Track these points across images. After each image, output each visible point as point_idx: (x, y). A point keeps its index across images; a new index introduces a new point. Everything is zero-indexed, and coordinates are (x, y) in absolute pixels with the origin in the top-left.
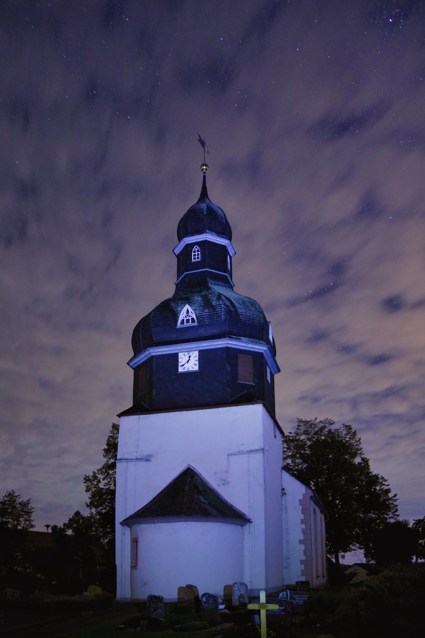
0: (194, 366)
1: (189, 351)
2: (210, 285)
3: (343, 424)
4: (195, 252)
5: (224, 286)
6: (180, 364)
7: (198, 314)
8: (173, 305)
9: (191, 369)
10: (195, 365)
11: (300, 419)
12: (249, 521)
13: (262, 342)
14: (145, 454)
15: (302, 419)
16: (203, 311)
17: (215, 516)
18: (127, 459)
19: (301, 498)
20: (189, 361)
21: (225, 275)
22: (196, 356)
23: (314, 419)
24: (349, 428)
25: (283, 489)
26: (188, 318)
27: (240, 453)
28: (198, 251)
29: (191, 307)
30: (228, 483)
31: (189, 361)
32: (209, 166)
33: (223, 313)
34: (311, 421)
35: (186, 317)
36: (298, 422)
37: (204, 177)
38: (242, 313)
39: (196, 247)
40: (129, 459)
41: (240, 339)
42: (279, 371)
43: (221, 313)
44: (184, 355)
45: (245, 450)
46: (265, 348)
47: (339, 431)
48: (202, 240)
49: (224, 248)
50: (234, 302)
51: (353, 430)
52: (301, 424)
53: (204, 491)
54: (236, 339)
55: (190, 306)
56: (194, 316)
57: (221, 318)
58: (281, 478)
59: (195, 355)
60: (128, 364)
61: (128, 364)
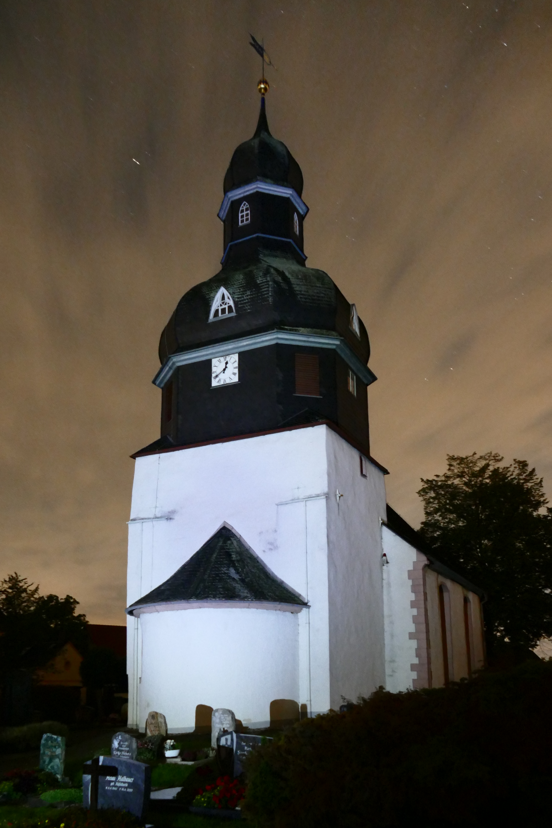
0: (232, 376)
1: (226, 354)
2: (261, 256)
3: (515, 460)
4: (242, 211)
5: (285, 257)
6: (214, 375)
7: (236, 299)
8: (205, 290)
9: (228, 381)
10: (234, 374)
11: (451, 455)
12: (305, 605)
13: (334, 333)
14: (167, 509)
15: (454, 456)
16: (244, 294)
17: (243, 599)
18: (143, 519)
19: (411, 568)
20: (225, 371)
21: (264, 234)
22: (235, 361)
23: (471, 454)
24: (523, 465)
25: (385, 555)
26: (223, 306)
27: (295, 500)
28: (247, 210)
29: (228, 291)
30: (276, 548)
31: (225, 371)
32: (268, 81)
33: (270, 294)
34: (467, 458)
35: (221, 305)
36: (448, 459)
37: (263, 100)
38: (301, 291)
39: (245, 204)
40: (145, 519)
41: (296, 330)
42: (374, 379)
43: (268, 294)
44: (220, 361)
45: (302, 497)
46: (338, 342)
47: (509, 469)
48: (252, 192)
49: (287, 200)
50: (289, 276)
51: (529, 469)
52: (455, 463)
53: (238, 561)
54: (290, 330)
55: (226, 289)
56: (231, 303)
57: (268, 301)
58: (382, 539)
59: (234, 360)
60: (154, 382)
61: (154, 382)
